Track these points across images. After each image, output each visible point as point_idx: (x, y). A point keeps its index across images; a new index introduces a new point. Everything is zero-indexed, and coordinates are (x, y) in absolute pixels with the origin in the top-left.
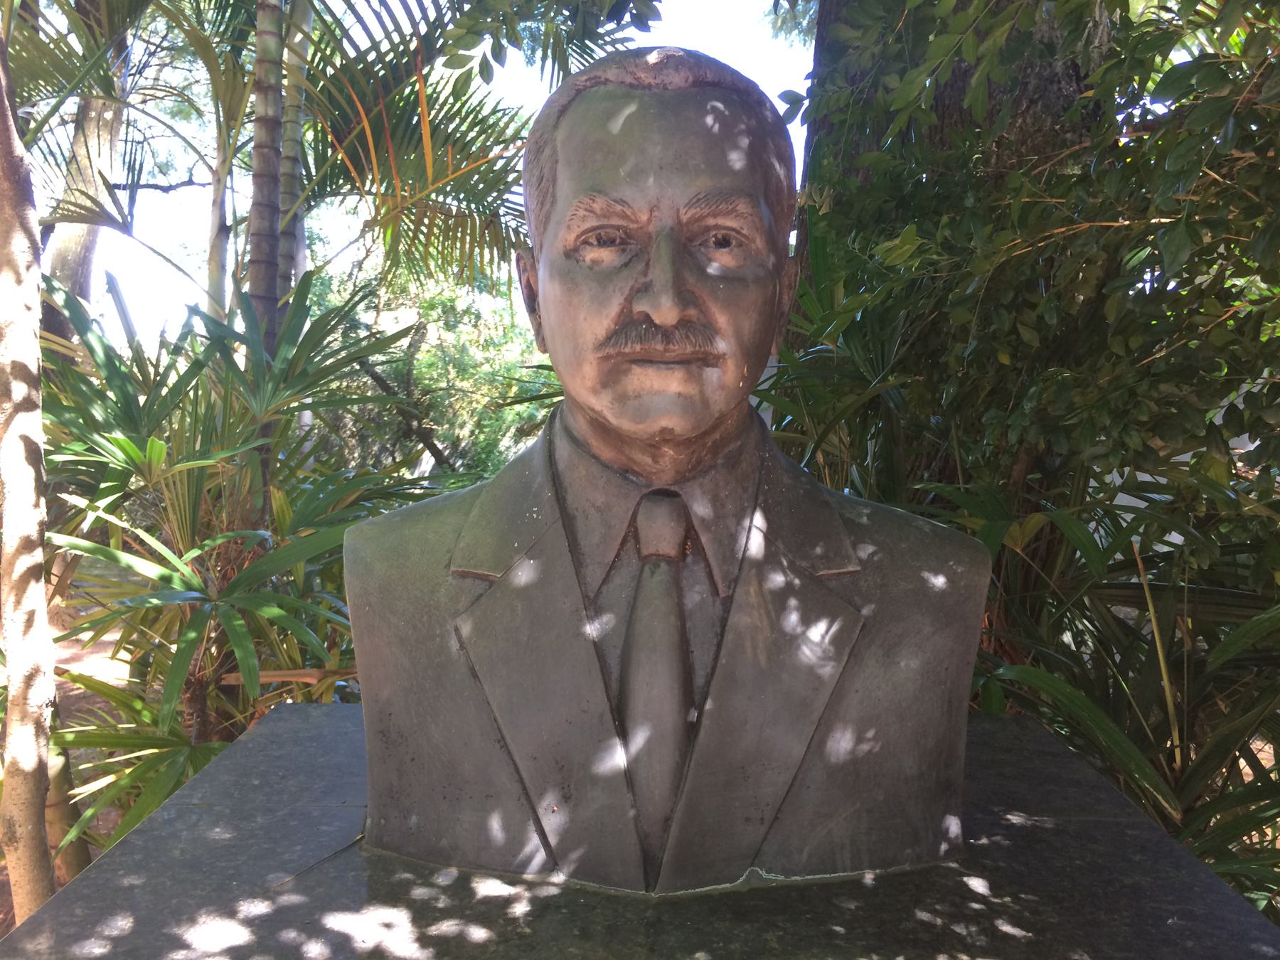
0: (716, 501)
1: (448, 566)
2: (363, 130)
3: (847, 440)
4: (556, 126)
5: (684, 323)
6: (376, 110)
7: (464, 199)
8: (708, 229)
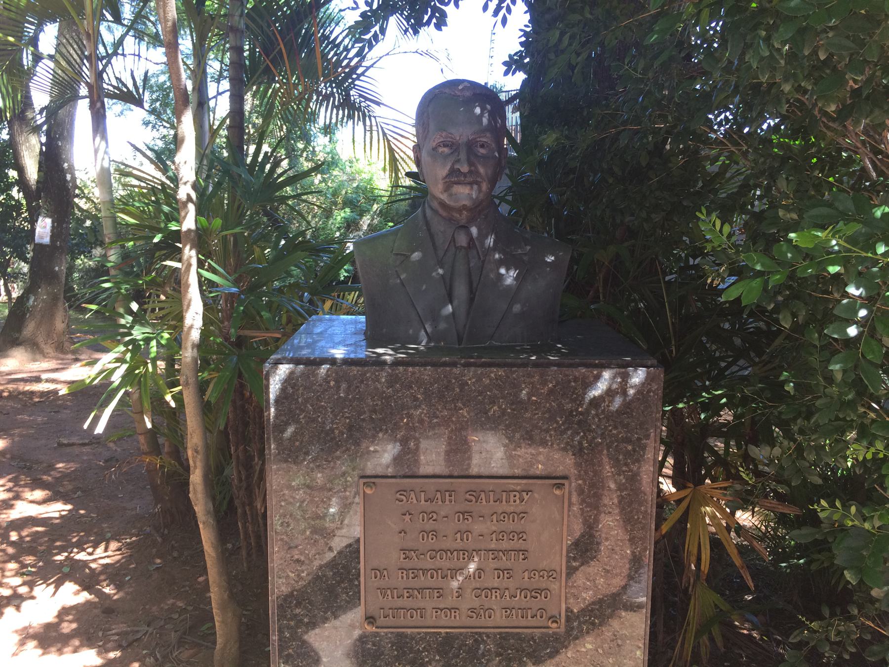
0: (479, 229)
1: (392, 252)
2: (281, 49)
3: (541, 220)
4: (428, 106)
5: (470, 172)
6: (288, 37)
7: (335, 87)
8: (477, 142)
